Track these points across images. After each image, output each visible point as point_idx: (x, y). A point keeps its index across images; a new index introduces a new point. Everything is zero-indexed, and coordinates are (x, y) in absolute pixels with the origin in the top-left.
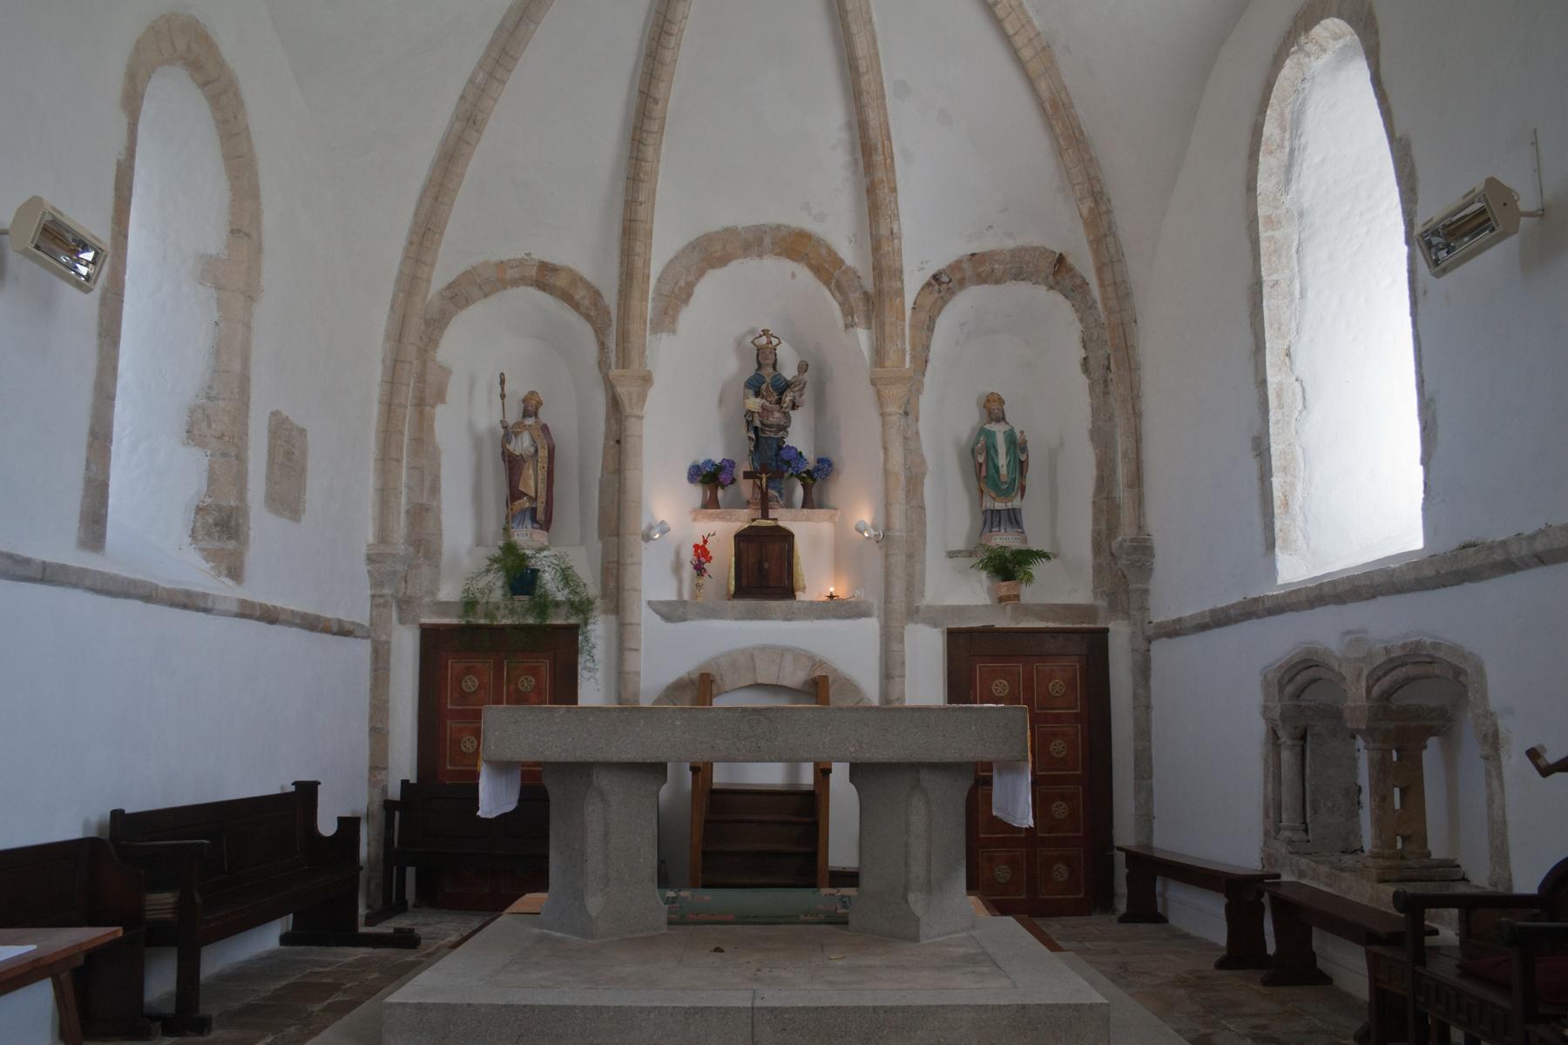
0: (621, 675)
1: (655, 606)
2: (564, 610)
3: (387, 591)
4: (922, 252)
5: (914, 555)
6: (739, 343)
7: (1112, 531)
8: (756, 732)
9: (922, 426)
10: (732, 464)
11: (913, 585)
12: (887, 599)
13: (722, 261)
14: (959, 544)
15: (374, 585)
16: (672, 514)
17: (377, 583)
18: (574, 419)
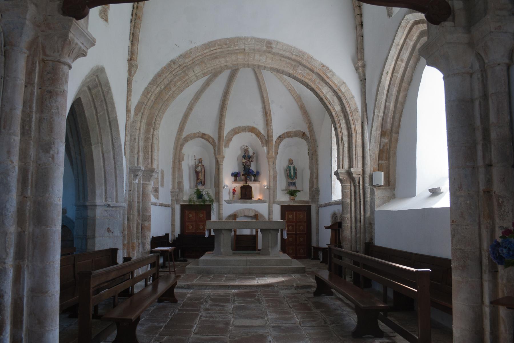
0: (219, 214)
1: (225, 201)
2: (208, 202)
3: (174, 198)
4: (277, 131)
5: (275, 191)
6: (241, 148)
7: (312, 186)
8: (245, 225)
9: (277, 166)
10: (240, 173)
11: (274, 197)
12: (269, 200)
13: (238, 133)
14: (284, 188)
15: (172, 197)
17: (172, 196)
18: (209, 163)
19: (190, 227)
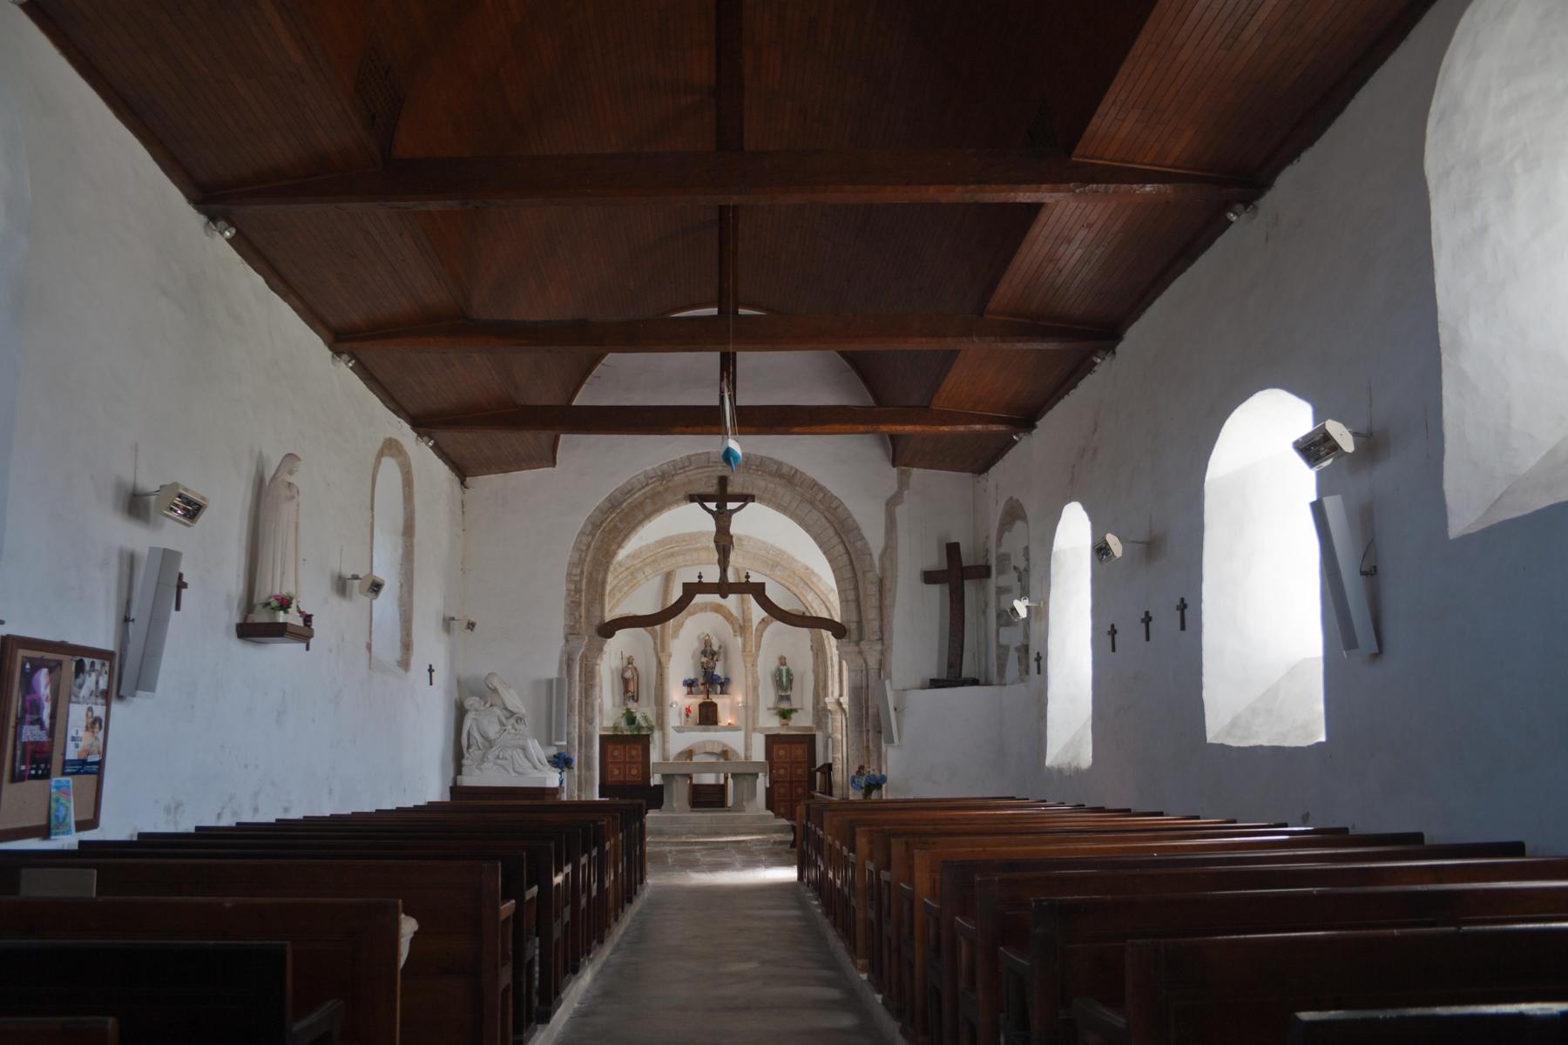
0: (664, 750)
5: (755, 710)
16: (679, 699)
18: (646, 664)
19: (616, 772)
